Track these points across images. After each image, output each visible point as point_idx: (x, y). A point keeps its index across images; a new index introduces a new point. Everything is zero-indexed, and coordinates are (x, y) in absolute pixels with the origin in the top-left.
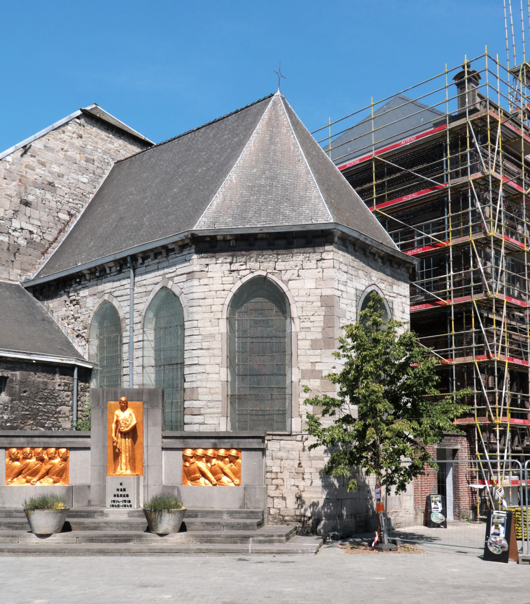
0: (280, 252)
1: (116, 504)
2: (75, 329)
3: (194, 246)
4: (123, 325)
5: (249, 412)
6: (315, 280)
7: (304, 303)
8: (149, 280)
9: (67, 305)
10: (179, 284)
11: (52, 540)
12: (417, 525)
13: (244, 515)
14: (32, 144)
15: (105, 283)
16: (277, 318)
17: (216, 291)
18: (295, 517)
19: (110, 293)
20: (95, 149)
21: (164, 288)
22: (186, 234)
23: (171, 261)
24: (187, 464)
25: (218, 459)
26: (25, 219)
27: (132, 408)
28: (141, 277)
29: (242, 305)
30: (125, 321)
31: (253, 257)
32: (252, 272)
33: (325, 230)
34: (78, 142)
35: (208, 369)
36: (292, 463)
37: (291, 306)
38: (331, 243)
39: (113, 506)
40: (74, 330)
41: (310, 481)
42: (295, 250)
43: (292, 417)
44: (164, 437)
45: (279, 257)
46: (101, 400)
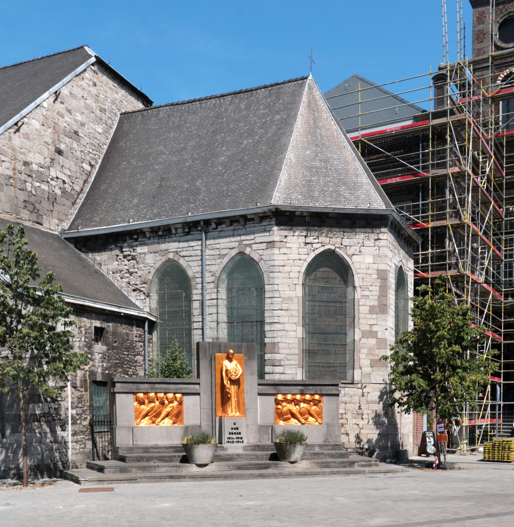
0: (346, 230)
1: (231, 440)
2: (131, 283)
3: (274, 219)
4: (193, 283)
5: (317, 364)
6: (373, 256)
7: (365, 275)
8: (223, 244)
9: (120, 259)
10: (258, 251)
11: (209, 469)
12: (414, 455)
13: (331, 447)
14: (61, 89)
15: (169, 242)
16: (340, 286)
17: (294, 260)
18: (356, 449)
19: (176, 252)
20: (106, 98)
21: (241, 253)
22: (271, 208)
23: (248, 229)
24: (280, 407)
25: (304, 403)
26: (59, 167)
27: (236, 360)
28: (213, 241)
29: (312, 273)
30: (195, 280)
31: (324, 233)
32: (323, 246)
33: (383, 215)
34: (94, 90)
35: (288, 327)
36: (354, 406)
37: (355, 276)
38: (385, 226)
39: (228, 442)
40: (129, 284)
41: (367, 421)
42: (358, 230)
43: (354, 369)
44: (259, 385)
45: (345, 234)
46: (208, 352)
